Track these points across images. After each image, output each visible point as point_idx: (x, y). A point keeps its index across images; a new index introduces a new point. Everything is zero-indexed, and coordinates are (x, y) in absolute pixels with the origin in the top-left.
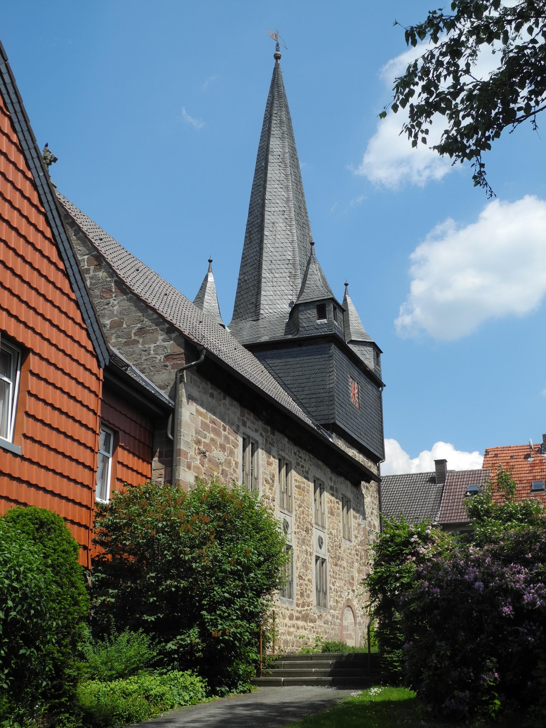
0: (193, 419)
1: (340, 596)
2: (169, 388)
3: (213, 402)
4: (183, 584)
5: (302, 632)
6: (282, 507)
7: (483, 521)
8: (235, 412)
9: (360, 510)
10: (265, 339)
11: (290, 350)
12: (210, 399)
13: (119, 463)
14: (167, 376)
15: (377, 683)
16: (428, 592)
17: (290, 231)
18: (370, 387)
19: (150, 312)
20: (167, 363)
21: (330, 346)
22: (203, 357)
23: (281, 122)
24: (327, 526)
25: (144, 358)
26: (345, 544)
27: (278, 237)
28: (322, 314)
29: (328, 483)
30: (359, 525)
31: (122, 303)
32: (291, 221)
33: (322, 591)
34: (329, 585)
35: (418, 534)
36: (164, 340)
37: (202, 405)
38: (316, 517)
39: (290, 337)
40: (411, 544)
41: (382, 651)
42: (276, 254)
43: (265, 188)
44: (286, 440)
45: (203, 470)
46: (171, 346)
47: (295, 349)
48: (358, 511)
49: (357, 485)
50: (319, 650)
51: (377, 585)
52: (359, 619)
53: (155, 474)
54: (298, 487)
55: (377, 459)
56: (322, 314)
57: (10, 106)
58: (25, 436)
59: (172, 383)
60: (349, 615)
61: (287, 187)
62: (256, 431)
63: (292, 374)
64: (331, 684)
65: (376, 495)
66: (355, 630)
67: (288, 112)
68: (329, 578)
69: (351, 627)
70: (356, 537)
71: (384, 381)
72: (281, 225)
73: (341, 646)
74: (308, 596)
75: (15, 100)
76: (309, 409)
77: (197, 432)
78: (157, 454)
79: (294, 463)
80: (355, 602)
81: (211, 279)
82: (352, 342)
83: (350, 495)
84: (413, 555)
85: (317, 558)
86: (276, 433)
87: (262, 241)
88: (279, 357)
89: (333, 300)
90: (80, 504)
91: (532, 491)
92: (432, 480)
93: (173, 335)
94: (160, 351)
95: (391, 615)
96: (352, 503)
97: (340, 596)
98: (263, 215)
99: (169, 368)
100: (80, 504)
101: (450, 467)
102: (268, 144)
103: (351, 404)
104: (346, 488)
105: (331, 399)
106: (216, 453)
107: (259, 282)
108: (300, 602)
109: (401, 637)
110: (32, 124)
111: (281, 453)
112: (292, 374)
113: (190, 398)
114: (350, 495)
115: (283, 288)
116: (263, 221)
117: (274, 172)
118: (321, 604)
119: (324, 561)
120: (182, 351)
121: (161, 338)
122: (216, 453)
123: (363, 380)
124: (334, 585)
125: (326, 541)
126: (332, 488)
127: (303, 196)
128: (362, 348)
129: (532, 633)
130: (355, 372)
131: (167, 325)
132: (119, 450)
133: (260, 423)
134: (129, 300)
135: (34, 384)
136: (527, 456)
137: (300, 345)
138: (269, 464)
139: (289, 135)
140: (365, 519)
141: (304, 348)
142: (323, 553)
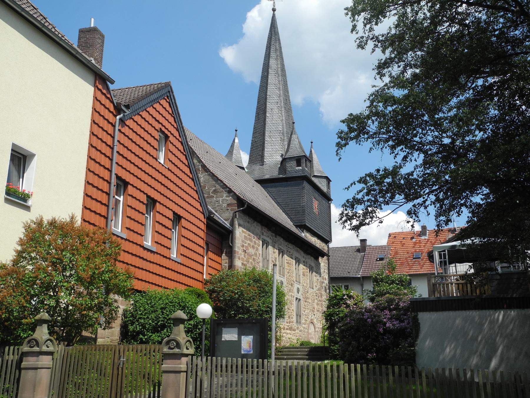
0: (241, 234)
1: (308, 318)
2: (230, 220)
3: (249, 225)
4: (246, 316)
5: (290, 336)
6: (280, 274)
7: (379, 284)
8: (258, 228)
9: (318, 272)
10: (267, 177)
11: (281, 183)
12: (248, 224)
13: (157, 222)
14: (229, 214)
15: (327, 359)
16: (349, 323)
17: (281, 114)
18: (324, 202)
19: (219, 182)
20: (228, 208)
21: (303, 182)
22: (246, 206)
23: (276, 50)
24: (301, 282)
25: (217, 205)
26: (311, 291)
27: (274, 117)
28: (299, 164)
29: (302, 259)
30: (318, 280)
31: (205, 177)
32: (281, 108)
33: (299, 316)
34: (302, 312)
35: (347, 295)
36: (226, 197)
37: (244, 228)
38: (296, 278)
39: (281, 176)
40: (344, 299)
41: (330, 345)
42: (273, 127)
43: (267, 88)
44: (282, 239)
45: (245, 259)
46: (230, 199)
47: (284, 183)
48: (317, 273)
49: (317, 259)
50: (298, 345)
51: (329, 316)
52: (317, 329)
53: (223, 263)
54: (288, 263)
55: (327, 241)
56: (299, 164)
57: (174, 114)
58: (181, 254)
59: (231, 218)
60: (312, 327)
61: (279, 88)
62: (268, 237)
63: (282, 197)
64: (308, 359)
65: (327, 261)
66: (315, 335)
67: (280, 43)
68: (302, 308)
69: (313, 333)
70: (316, 286)
71: (332, 198)
72: (276, 110)
73: (309, 343)
74: (292, 318)
75: (176, 109)
76: (292, 217)
77: (243, 241)
78: (224, 252)
79: (286, 251)
80: (315, 321)
81: (237, 141)
82: (315, 176)
83: (313, 265)
84: (344, 304)
85: (297, 299)
86: (278, 237)
87: (265, 119)
88: (275, 187)
89: (305, 156)
90: (199, 281)
91: (414, 258)
92: (358, 251)
93: (231, 194)
94: (225, 202)
95: (334, 330)
96: (315, 269)
97: (308, 318)
98: (266, 105)
99: (230, 210)
100: (199, 281)
101: (368, 243)
102: (269, 62)
103: (314, 213)
104: (311, 261)
105: (304, 211)
106: (251, 251)
107: (264, 143)
108: (288, 321)
109: (338, 339)
110: (181, 117)
111: (280, 247)
112: (282, 197)
113: (239, 225)
114: (313, 265)
115: (277, 147)
116: (266, 107)
117: (272, 79)
118: (298, 322)
119: (300, 300)
120: (236, 202)
121: (225, 195)
122: (251, 251)
123: (321, 198)
124: (305, 312)
125: (301, 289)
126: (304, 262)
127: (288, 93)
128: (320, 180)
129: (388, 338)
130: (316, 194)
131: (228, 189)
132: (209, 252)
133: (270, 232)
134: (209, 175)
135: (184, 232)
136: (412, 238)
137: (287, 181)
138: (274, 253)
139: (280, 57)
140: (320, 276)
141: (289, 183)
142: (300, 296)
